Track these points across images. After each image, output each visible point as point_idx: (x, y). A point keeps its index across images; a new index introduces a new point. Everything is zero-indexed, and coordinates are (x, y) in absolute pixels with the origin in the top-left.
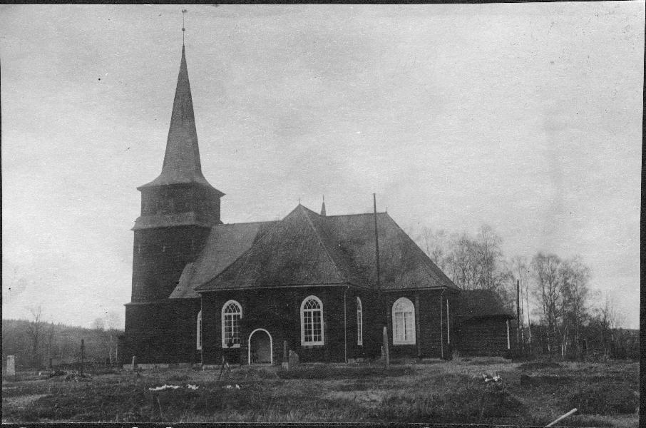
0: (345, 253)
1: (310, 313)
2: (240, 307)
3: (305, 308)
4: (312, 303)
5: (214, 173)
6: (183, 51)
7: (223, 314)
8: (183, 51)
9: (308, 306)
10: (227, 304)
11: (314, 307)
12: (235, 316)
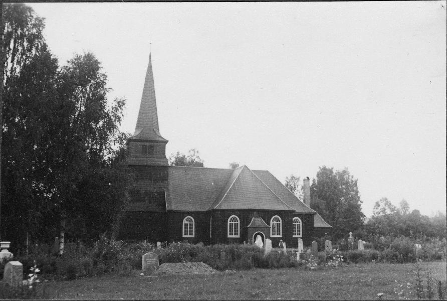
0: (411, 220)
1: (232, 224)
2: (193, 220)
3: (230, 221)
4: (234, 219)
5: (164, 132)
6: (150, 56)
7: (229, 222)
8: (150, 56)
9: (233, 220)
10: (188, 217)
11: (235, 221)
12: (235, 224)
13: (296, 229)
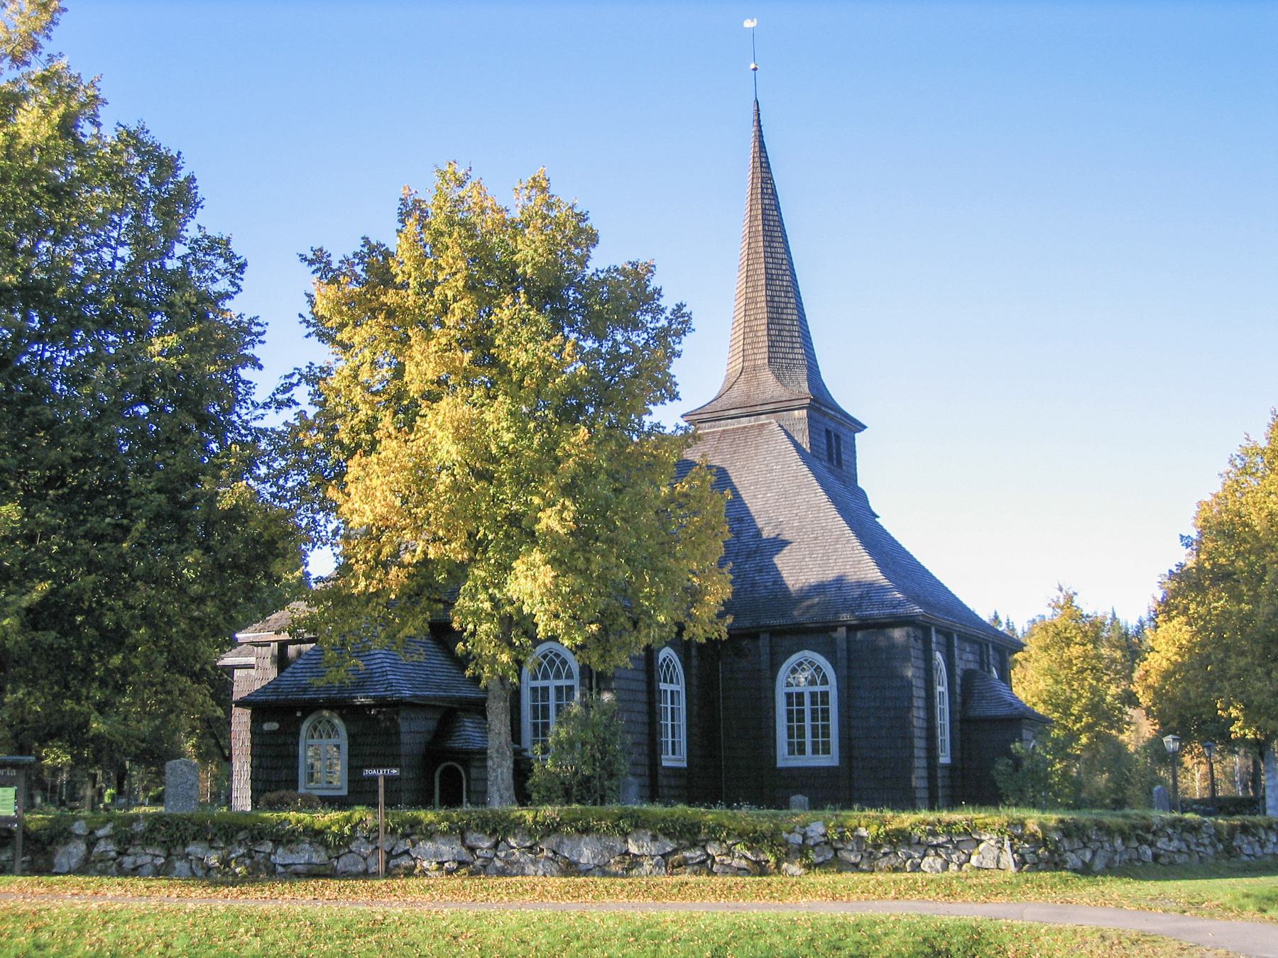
13: (808, 723)
